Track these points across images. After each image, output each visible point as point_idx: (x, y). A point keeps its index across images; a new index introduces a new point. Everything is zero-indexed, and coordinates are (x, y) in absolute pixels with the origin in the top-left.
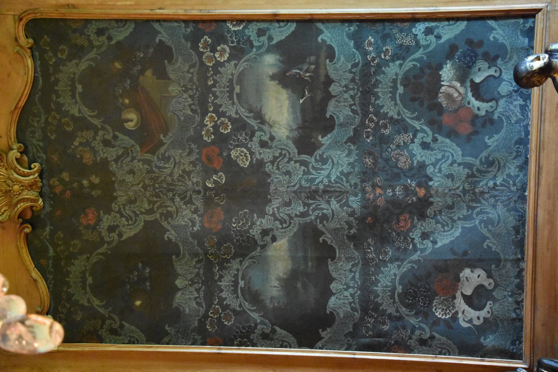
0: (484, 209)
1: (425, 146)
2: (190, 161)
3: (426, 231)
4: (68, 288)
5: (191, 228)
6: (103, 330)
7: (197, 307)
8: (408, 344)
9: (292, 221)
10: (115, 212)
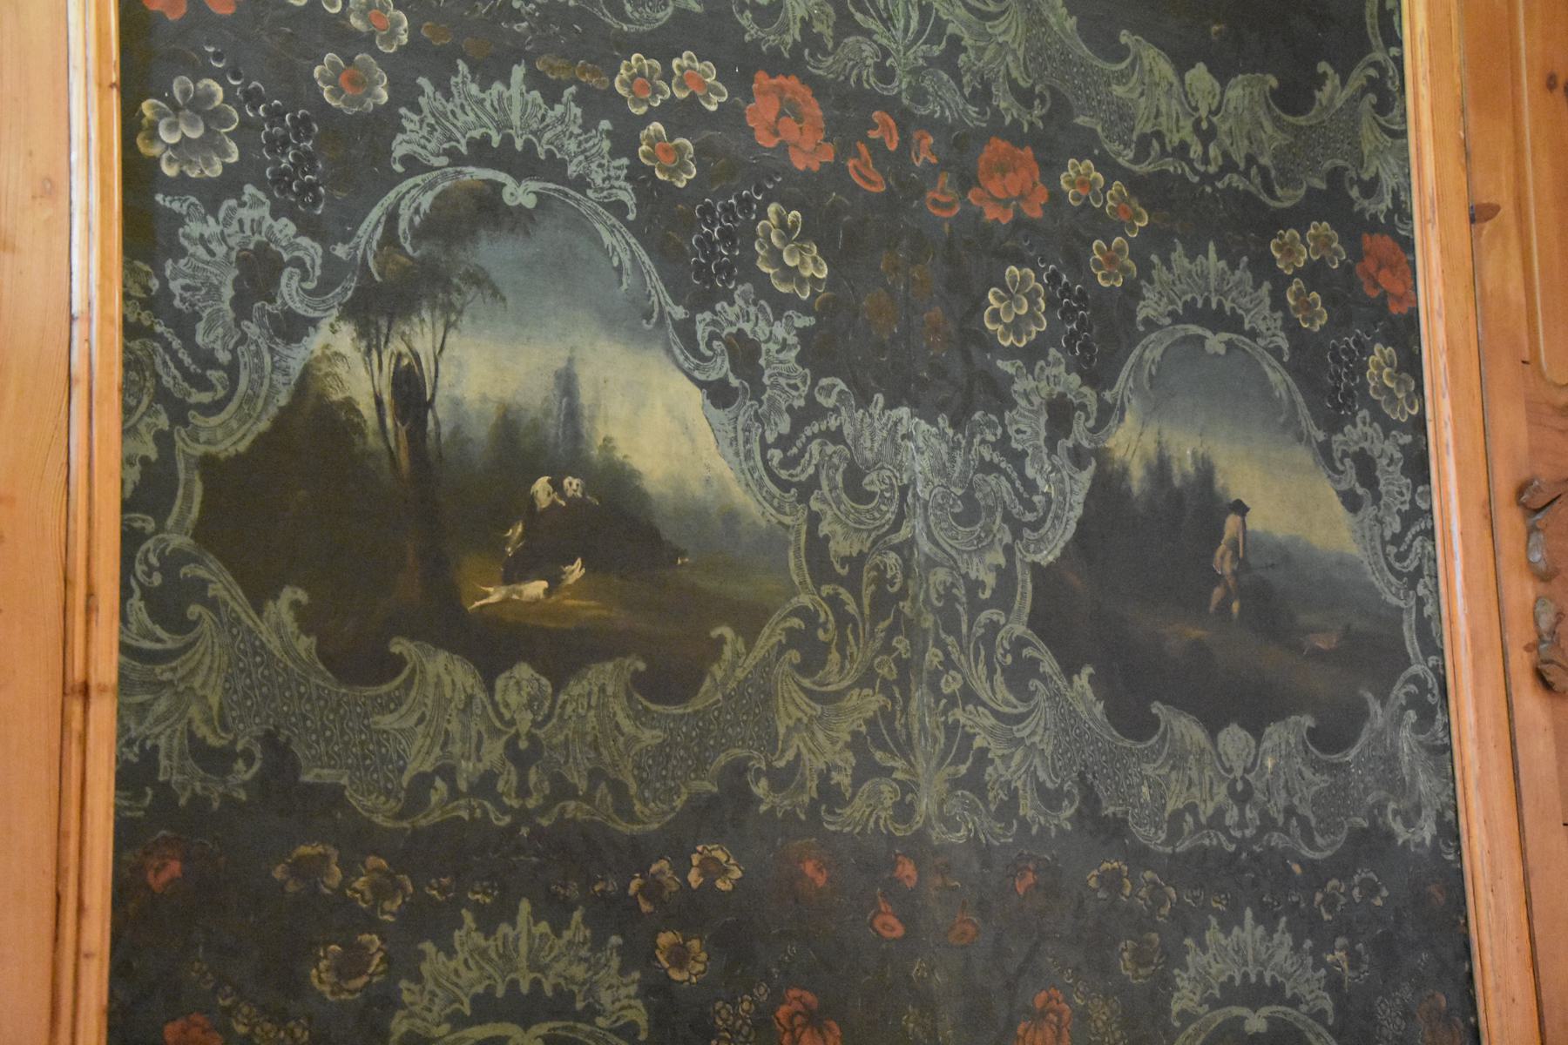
0: (855, 632)
4: (478, 909)
5: (764, 767)
6: (265, 211)
7: (405, 783)
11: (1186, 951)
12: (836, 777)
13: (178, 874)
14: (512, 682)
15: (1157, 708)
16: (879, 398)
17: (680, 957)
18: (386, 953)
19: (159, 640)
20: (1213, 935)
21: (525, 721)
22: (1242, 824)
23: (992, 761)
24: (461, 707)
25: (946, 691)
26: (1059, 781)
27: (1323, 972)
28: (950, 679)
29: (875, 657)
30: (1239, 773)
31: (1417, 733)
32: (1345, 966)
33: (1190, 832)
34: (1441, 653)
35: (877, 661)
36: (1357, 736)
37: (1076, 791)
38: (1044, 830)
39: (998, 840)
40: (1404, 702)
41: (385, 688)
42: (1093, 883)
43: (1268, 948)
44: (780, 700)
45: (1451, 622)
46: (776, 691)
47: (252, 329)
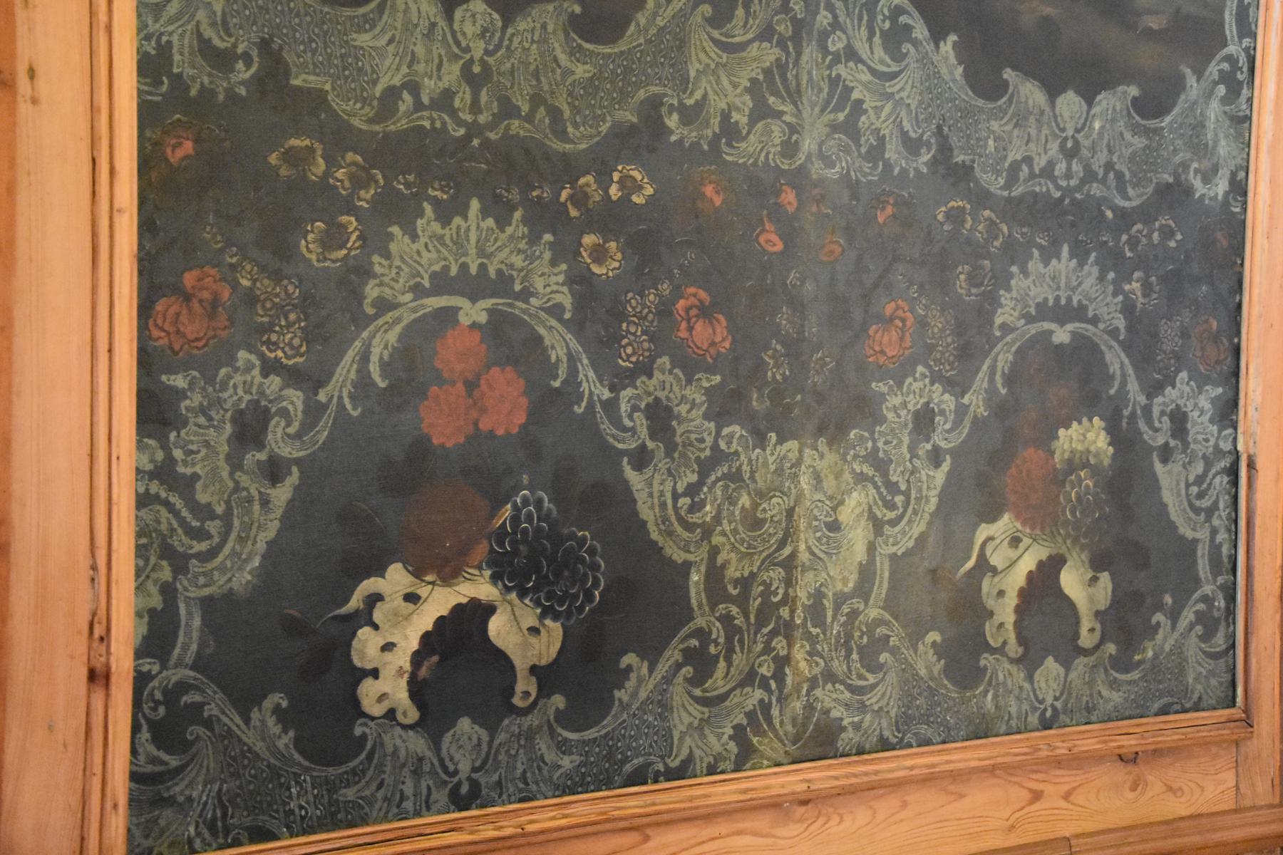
0: (741, 642)
1: (924, 420)
2: (884, 136)
4: (436, 203)
5: (676, 103)
8: (243, 355)
11: (1012, 276)
12: (736, 116)
13: (191, 152)
14: (468, 15)
15: (1008, 74)
16: (773, 437)
17: (600, 254)
18: (361, 232)
20: (1035, 265)
21: (478, 48)
22: (1068, 175)
23: (866, 111)
24: (425, 32)
25: (832, 48)
26: (920, 131)
27: (1120, 298)
28: (836, 39)
29: (775, 15)
30: (1070, 132)
31: (1224, 105)
32: (1139, 294)
33: (1024, 180)
34: (1254, 36)
35: (776, 18)
36: (1174, 104)
37: (933, 141)
38: (904, 172)
39: (864, 177)
40: (1217, 78)
41: (361, 11)
42: (940, 217)
43: (1078, 277)
44: (693, 47)
45: (1267, 9)
46: (690, 38)
47: (244, 480)
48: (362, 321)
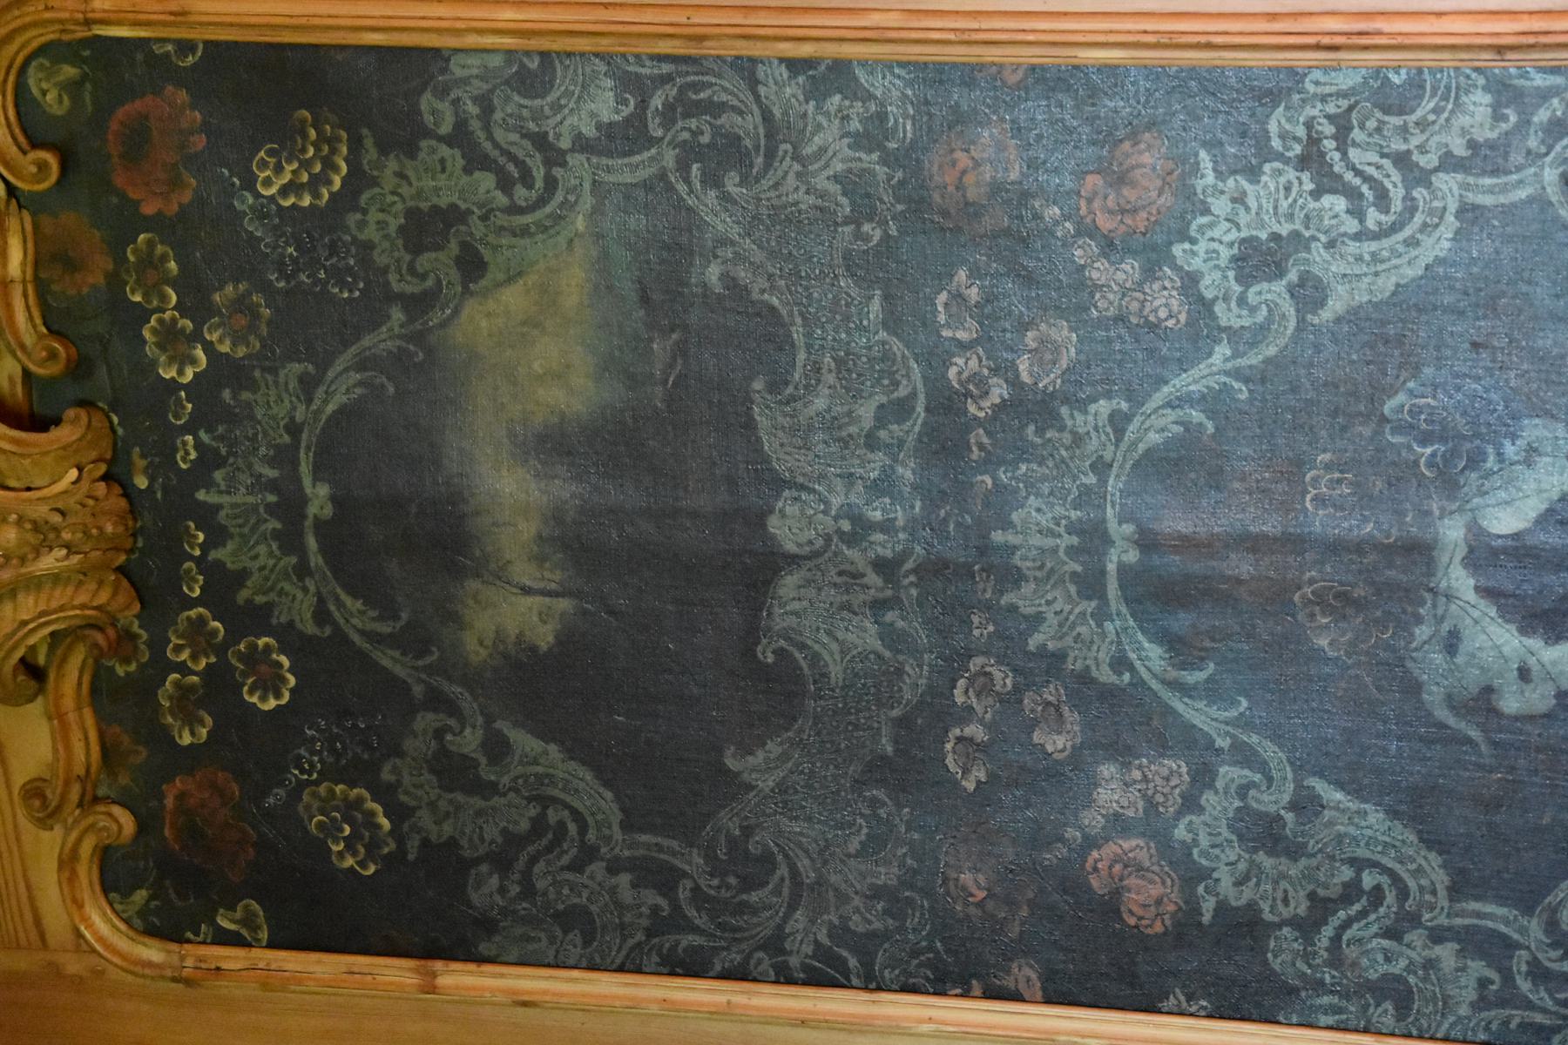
3: (1264, 236)
5: (848, 229)
9: (558, 172)
10: (440, 139)
19: (782, 879)
48: (340, 638)
